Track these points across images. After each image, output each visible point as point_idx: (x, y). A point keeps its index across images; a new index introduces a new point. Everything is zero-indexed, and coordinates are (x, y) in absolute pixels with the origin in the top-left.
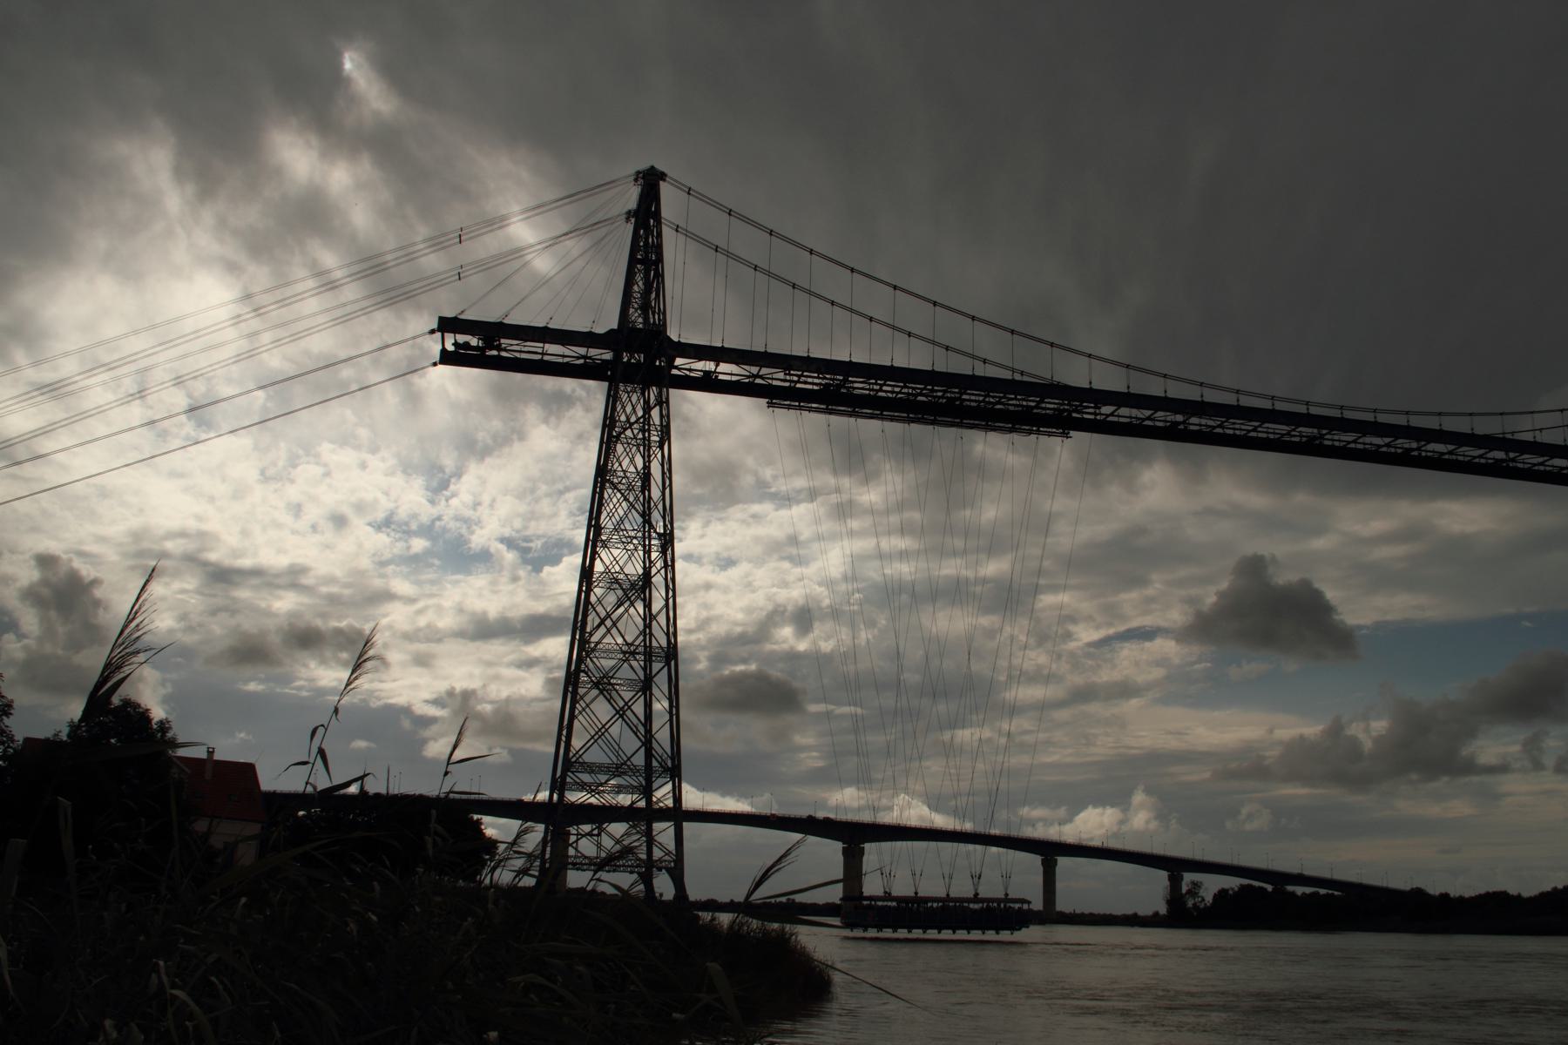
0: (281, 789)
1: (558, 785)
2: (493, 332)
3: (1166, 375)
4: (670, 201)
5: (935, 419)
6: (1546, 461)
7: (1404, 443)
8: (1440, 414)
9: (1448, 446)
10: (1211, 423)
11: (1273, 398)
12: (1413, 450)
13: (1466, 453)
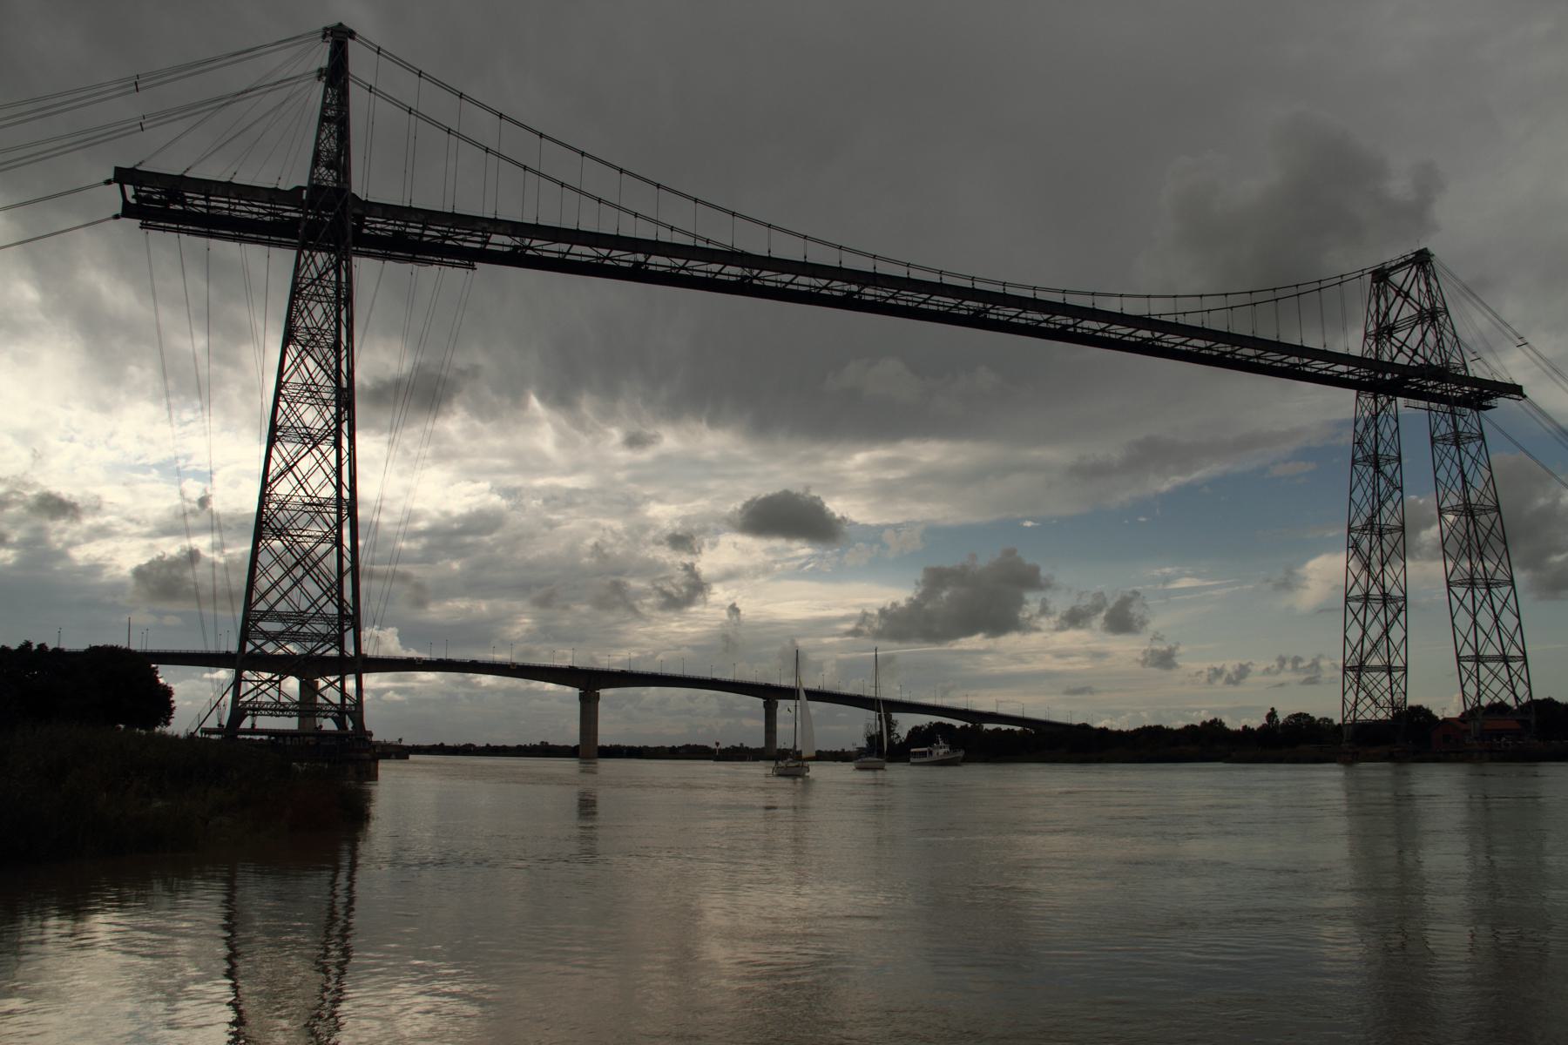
0: (582, 665)
1: (245, 636)
2: (176, 186)
3: (875, 256)
4: (359, 60)
5: (414, 257)
6: (1020, 313)
7: (1061, 319)
8: (1093, 294)
9: (1100, 323)
10: (884, 294)
11: (941, 272)
12: (1069, 326)
13: (622, 258)
